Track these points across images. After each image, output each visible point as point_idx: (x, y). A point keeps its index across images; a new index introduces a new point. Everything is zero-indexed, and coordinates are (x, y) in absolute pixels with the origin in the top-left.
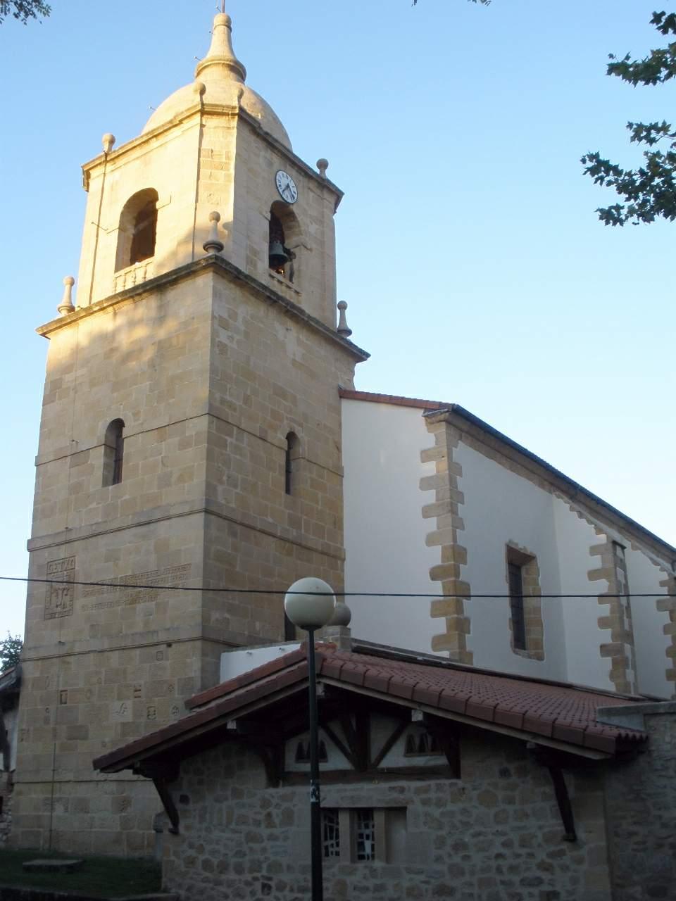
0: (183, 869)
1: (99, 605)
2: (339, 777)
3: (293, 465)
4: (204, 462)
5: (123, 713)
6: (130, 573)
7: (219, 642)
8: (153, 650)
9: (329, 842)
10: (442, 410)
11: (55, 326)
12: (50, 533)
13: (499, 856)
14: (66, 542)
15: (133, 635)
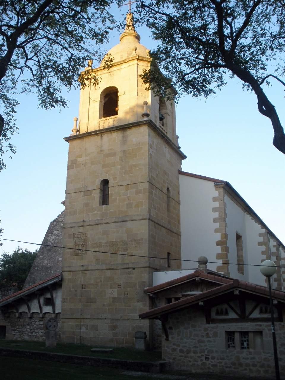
4: (147, 200)
5: (112, 294)
6: (114, 240)
8: (127, 271)
10: (222, 183)
11: (73, 138)
12: (74, 222)
14: (83, 226)
15: (117, 264)
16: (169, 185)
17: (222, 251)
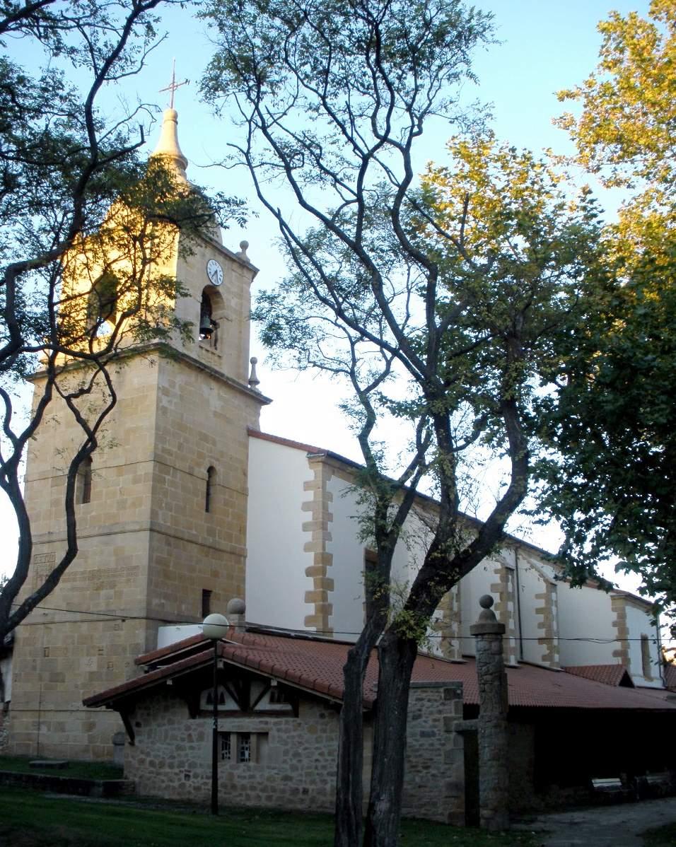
0: (137, 766)
1: (73, 589)
2: (231, 714)
3: (212, 491)
4: (150, 495)
7: (159, 620)
8: (112, 624)
9: (224, 752)
13: (317, 760)
16: (213, 460)
17: (315, 587)
